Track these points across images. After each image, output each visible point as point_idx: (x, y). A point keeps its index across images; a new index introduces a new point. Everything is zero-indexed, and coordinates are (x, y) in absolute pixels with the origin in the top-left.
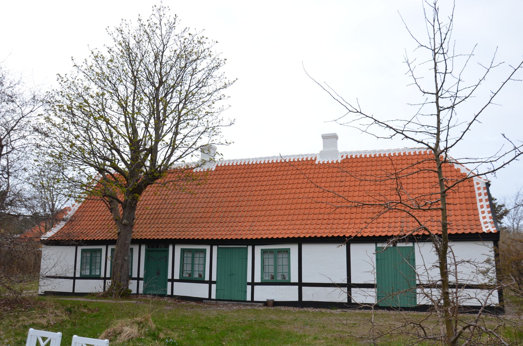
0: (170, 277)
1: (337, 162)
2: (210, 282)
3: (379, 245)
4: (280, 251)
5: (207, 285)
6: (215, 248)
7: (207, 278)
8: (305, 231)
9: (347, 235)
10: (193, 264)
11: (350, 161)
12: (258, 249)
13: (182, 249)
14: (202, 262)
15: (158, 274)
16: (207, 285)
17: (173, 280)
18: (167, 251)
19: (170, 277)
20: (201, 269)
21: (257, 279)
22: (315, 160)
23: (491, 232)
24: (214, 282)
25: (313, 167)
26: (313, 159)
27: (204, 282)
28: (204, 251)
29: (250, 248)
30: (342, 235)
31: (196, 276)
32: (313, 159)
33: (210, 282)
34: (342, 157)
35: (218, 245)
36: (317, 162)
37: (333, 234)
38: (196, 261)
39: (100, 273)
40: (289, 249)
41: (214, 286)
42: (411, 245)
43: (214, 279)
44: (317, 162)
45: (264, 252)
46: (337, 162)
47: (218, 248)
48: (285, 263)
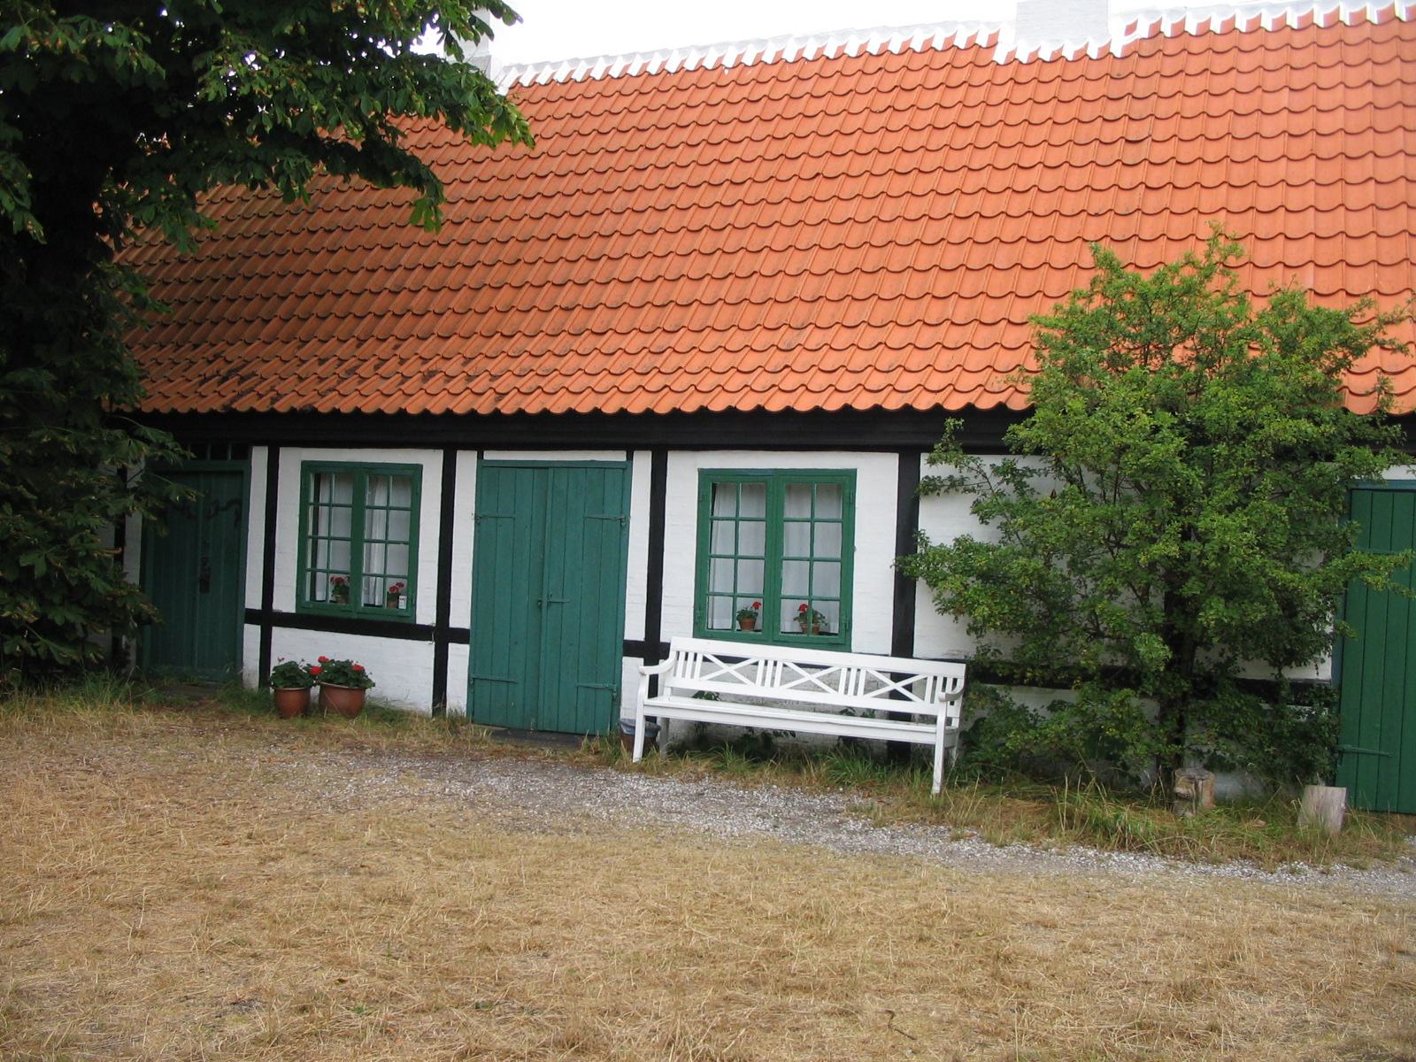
0: (253, 600)
1: (1106, 54)
2: (442, 635)
3: (489, 456)
4: (378, 474)
5: (426, 649)
6: (467, 464)
7: (426, 614)
8: (936, 381)
9: (955, 403)
10: (357, 540)
11: (1195, 46)
12: (685, 471)
13: (704, 474)
14: (399, 532)
15: (205, 584)
16: (426, 649)
17: (268, 619)
18: (243, 476)
19: (253, 600)
20: (397, 567)
21: (285, 601)
22: (992, 46)
23: (315, 410)
24: (461, 636)
25: (980, 76)
26: (982, 41)
27: (419, 633)
28: (411, 478)
29: (642, 465)
30: (924, 403)
31: (373, 594)
32: (982, 41)
33: (442, 635)
34: (1131, 29)
35: (480, 448)
36: (1000, 56)
37: (906, 399)
38: (795, 539)
39: (412, 603)
40: (851, 475)
41: (459, 655)
42: (621, 456)
43: (460, 617)
44: (1000, 56)
45: (712, 485)
46: (1106, 54)
47: (483, 467)
48: (828, 543)
